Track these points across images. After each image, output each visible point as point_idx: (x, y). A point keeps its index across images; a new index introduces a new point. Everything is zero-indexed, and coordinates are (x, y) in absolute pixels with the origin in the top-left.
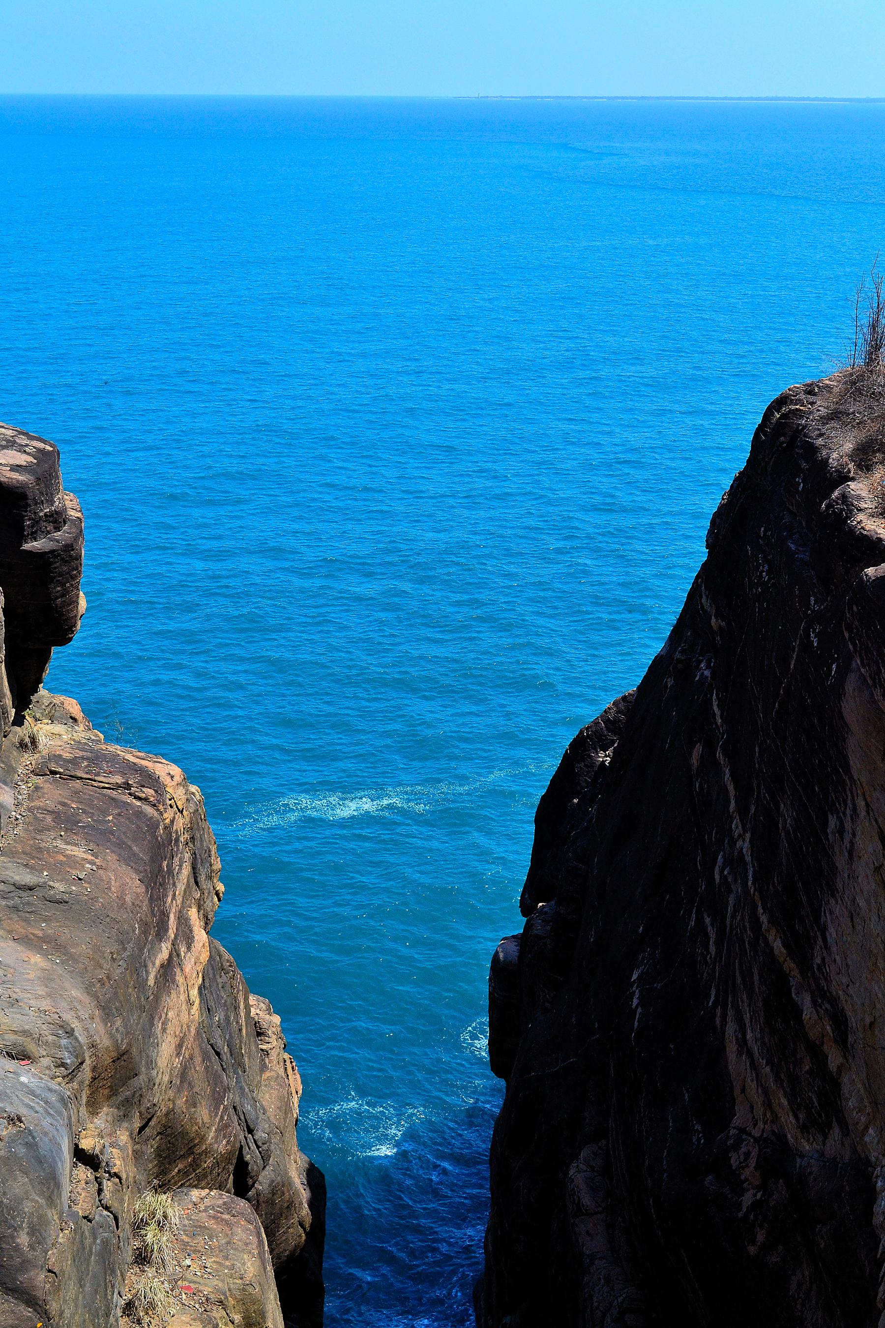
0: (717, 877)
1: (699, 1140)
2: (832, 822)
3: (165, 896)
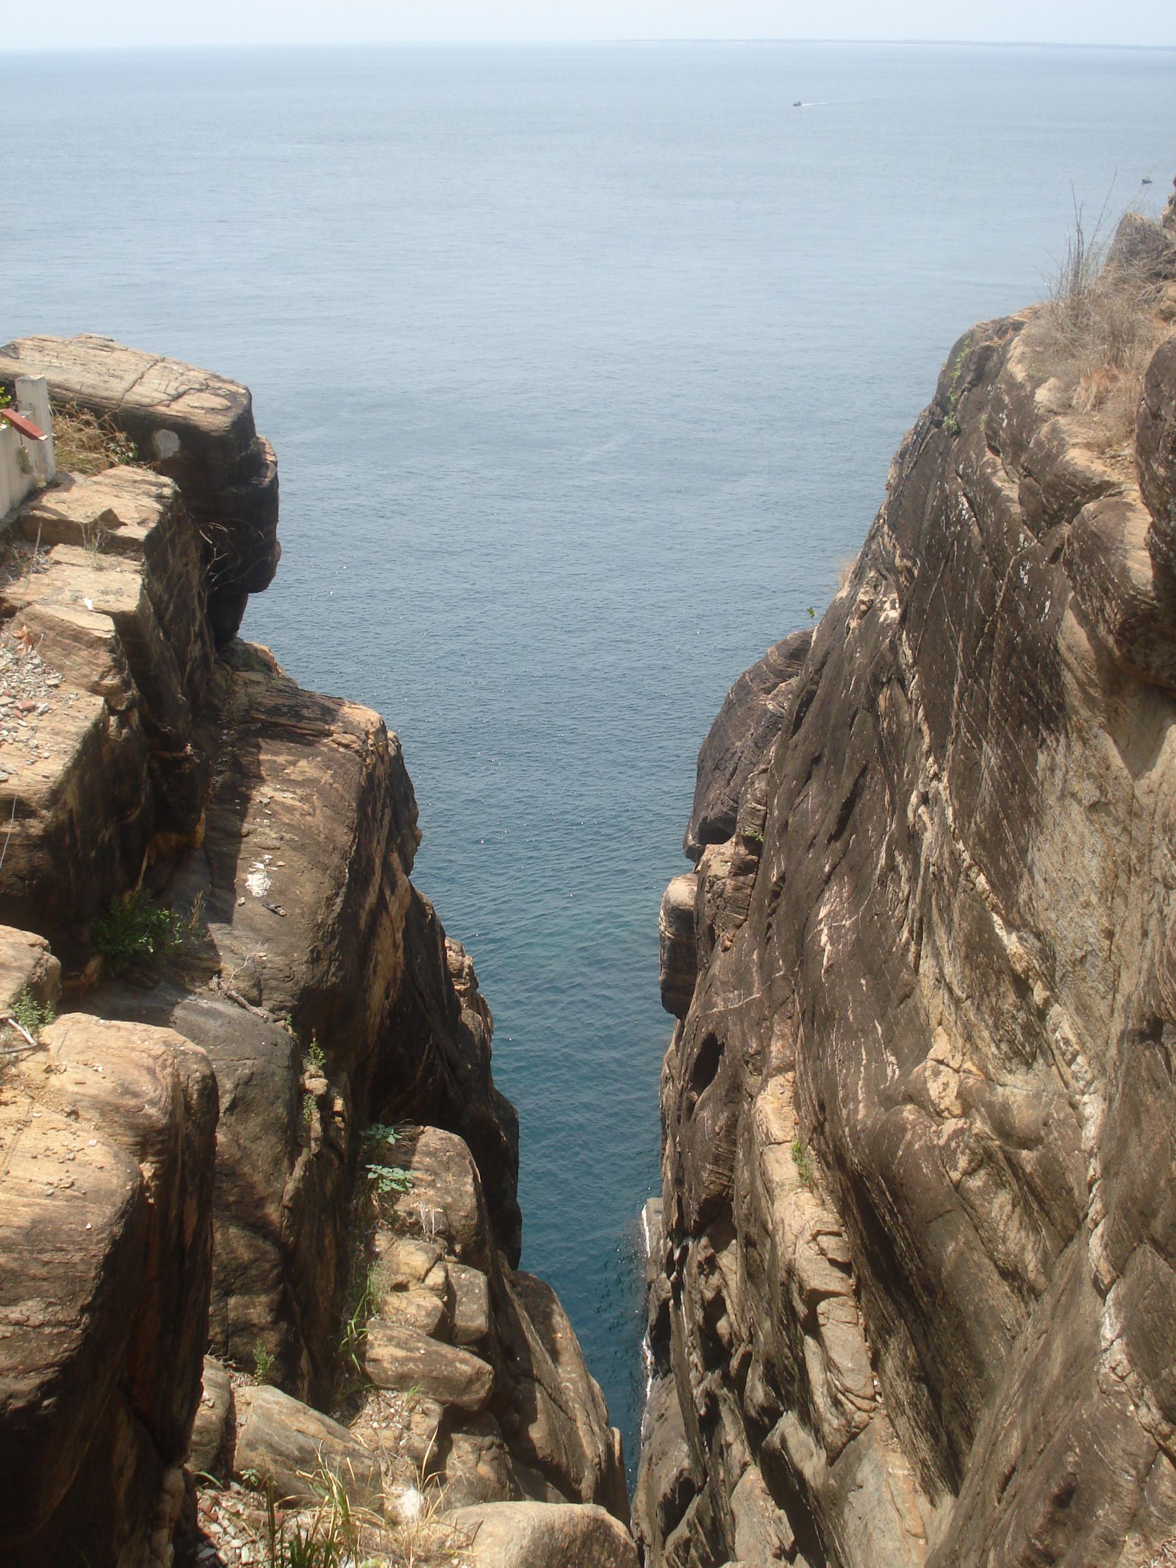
0: (910, 814)
1: (894, 1072)
2: (1042, 758)
3: (371, 841)
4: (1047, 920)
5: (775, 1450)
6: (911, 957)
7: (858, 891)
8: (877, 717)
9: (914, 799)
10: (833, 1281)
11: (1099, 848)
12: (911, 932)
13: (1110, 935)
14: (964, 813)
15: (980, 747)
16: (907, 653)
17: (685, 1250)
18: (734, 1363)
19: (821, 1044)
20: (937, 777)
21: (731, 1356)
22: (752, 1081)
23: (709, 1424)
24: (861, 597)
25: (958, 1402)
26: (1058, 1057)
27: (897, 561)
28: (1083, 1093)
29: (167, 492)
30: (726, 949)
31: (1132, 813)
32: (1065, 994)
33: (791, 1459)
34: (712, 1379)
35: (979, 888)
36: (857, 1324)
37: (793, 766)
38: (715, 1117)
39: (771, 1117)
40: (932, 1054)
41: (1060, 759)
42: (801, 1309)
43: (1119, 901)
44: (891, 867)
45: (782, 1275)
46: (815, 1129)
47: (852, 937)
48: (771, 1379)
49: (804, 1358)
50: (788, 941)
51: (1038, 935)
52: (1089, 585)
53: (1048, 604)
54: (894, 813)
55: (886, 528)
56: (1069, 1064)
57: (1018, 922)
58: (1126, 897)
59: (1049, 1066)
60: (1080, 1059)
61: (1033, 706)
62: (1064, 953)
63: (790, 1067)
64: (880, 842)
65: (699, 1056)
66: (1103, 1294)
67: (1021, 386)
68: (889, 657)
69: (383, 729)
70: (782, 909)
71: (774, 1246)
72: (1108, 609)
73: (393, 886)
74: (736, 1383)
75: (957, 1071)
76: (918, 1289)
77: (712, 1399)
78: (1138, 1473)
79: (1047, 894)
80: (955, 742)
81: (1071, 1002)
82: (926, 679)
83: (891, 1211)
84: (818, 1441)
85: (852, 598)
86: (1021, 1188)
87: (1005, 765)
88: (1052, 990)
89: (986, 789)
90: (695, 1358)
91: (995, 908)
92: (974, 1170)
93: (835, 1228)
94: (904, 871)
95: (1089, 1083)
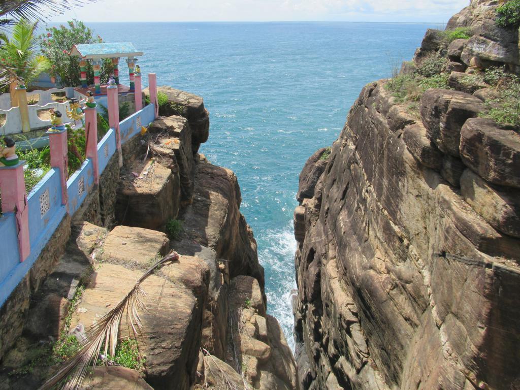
2: (400, 184)
4: (406, 223)
5: (339, 369)
6: (367, 230)
7: (350, 213)
8: (351, 171)
9: (364, 191)
10: (353, 319)
11: (419, 206)
12: (366, 224)
13: (426, 228)
14: (379, 196)
15: (382, 179)
16: (358, 156)
17: (307, 306)
18: (324, 340)
19: (344, 252)
20: (369, 186)
21: (323, 338)
22: (324, 261)
23: (317, 359)
24: (343, 142)
25: (396, 357)
26: (414, 259)
27: (352, 135)
28: (422, 269)
29: (185, 121)
30: (314, 226)
31: (428, 198)
32: (414, 243)
33: (344, 371)
34: (317, 345)
35: (385, 214)
36: (361, 331)
37: (329, 181)
38: (315, 270)
39: (332, 271)
40: (376, 256)
41: (405, 184)
42: (345, 326)
43: (427, 220)
44: (359, 207)
45: (338, 316)
46: (344, 275)
47: (350, 225)
48: (336, 347)
49: (346, 341)
50: (331, 225)
51: (404, 227)
52: (411, 144)
53: (398, 148)
54: (358, 194)
55: (348, 127)
56: (417, 261)
57: (398, 223)
58: (429, 219)
59: (411, 261)
60: (420, 260)
61: (397, 169)
62: (412, 232)
63: (335, 257)
64: (354, 201)
65: (309, 254)
66: (439, 328)
67: (384, 98)
68: (353, 157)
69: (233, 175)
70: (329, 217)
71: (335, 307)
72: (417, 150)
73: (236, 214)
74: (325, 347)
75: (384, 261)
76: (380, 322)
77: (318, 352)
78: (461, 385)
79: (405, 217)
80: (374, 178)
81: (415, 244)
82: (365, 163)
83: (369, 299)
84: (352, 366)
85: (341, 143)
86: (407, 294)
87: (389, 184)
88: (409, 241)
89: (385, 190)
90: (312, 338)
91: (390, 219)
92: (393, 289)
93: (351, 303)
94: (362, 208)
95: (424, 267)
